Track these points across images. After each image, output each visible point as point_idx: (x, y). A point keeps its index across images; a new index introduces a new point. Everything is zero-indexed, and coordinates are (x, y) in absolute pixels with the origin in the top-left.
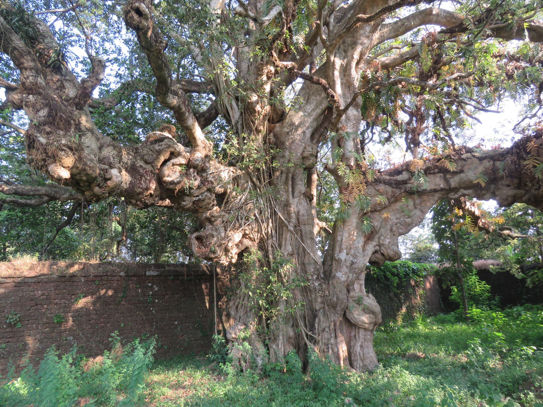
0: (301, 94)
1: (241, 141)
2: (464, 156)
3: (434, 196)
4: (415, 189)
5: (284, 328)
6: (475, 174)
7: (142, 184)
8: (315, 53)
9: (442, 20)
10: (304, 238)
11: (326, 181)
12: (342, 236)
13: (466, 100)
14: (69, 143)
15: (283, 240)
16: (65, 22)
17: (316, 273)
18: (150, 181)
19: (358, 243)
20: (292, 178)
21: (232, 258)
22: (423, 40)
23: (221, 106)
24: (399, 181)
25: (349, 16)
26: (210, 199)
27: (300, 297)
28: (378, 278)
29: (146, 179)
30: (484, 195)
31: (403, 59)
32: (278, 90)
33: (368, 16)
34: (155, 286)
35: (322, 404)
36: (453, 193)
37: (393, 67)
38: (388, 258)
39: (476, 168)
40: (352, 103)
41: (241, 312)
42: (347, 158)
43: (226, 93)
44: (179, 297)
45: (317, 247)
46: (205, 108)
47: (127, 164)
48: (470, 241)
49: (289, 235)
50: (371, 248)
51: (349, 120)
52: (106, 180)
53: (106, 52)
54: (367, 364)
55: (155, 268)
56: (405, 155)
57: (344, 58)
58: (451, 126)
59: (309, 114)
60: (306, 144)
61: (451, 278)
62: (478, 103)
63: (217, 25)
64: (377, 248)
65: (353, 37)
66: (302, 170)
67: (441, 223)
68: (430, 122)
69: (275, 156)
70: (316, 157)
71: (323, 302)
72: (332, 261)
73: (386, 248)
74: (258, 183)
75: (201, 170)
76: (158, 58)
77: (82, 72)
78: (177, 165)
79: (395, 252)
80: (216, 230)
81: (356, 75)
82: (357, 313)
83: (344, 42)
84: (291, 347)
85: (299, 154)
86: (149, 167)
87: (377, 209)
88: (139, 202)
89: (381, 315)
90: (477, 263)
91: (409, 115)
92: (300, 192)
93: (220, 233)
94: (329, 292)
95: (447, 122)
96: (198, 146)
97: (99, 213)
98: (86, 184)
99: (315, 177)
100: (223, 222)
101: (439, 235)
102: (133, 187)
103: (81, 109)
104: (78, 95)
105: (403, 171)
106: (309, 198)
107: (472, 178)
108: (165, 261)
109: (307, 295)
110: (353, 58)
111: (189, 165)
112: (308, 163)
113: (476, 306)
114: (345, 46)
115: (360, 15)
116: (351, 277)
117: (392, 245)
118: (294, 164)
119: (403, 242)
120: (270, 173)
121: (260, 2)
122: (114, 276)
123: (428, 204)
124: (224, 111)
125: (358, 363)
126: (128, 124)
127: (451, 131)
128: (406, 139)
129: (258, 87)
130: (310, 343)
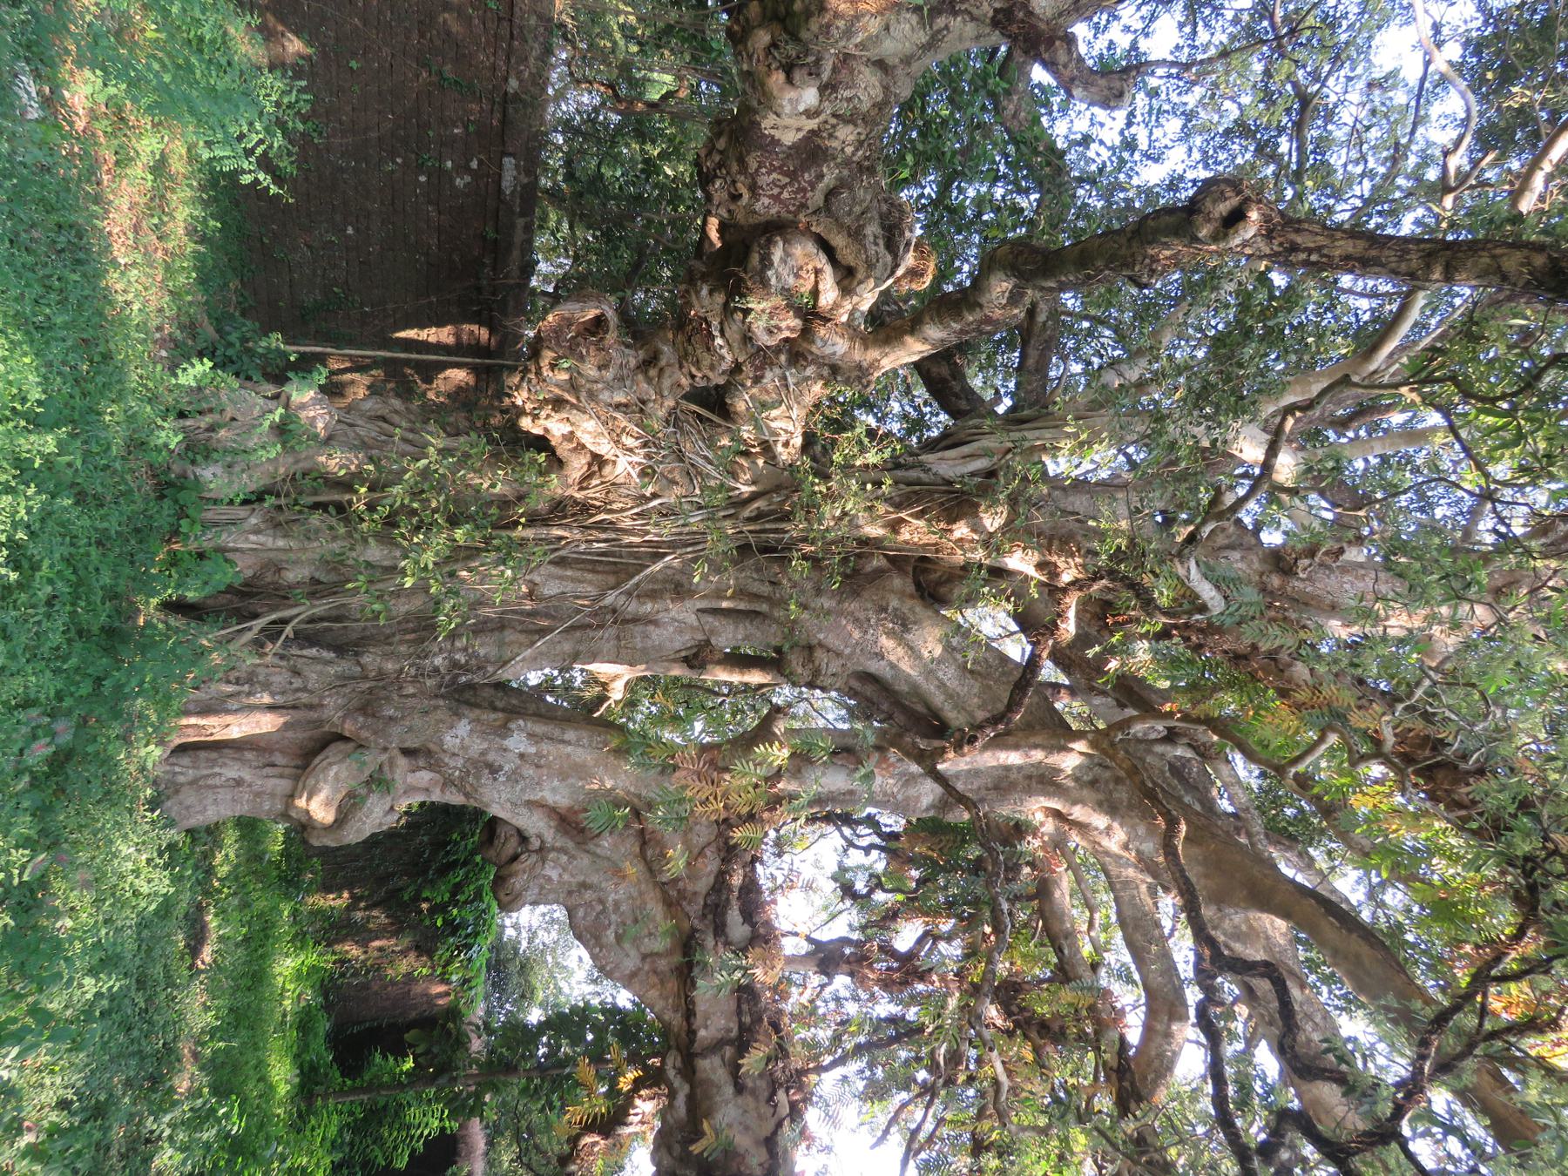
2: (781, 1096)
3: (676, 1011)
4: (698, 957)
5: (309, 555)
6: (730, 1126)
7: (769, 173)
8: (1098, 701)
9: (1153, 1045)
10: (578, 634)
11: (743, 712)
12: (578, 744)
13: (938, 1105)
15: (578, 574)
16: (1246, 17)
17: (473, 662)
18: (776, 198)
19: (554, 790)
20: (757, 613)
21: (535, 417)
22: (1106, 993)
23: (976, 427)
24: (724, 914)
25: (1187, 799)
26: (712, 367)
27: (403, 609)
29: (783, 187)
30: (670, 1150)
31: (1056, 937)
32: (1005, 590)
34: (468, 179)
35: (58, 648)
36: (679, 1064)
37: (1041, 913)
38: (504, 872)
39: (747, 1128)
40: (952, 794)
41: (367, 431)
42: (799, 771)
43: (1010, 445)
44: (429, 247)
46: (977, 382)
47: (831, 136)
48: (542, 1110)
49: (591, 590)
50: (536, 824)
51: (906, 784)
52: (788, 69)
54: (181, 797)
55: (524, 187)
56: (796, 934)
57: (1077, 779)
58: (871, 1065)
59: (931, 672)
60: (850, 657)
61: (436, 1056)
62: (930, 1139)
63: (1194, 437)
64: (536, 844)
65: (1130, 807)
66: (774, 642)
67: (599, 1030)
68: (885, 1008)
69: (821, 569)
70: (811, 685)
71: (381, 675)
72: (503, 710)
74: (746, 513)
75: (796, 352)
76: (1112, 259)
77: (1106, 44)
78: (817, 283)
79: (519, 895)
80: (620, 379)
81: (1036, 809)
82: (344, 774)
83: (1118, 780)
84: (249, 573)
85: (821, 636)
86: (816, 198)
87: (648, 846)
88: (717, 158)
89: (333, 844)
90: (477, 1134)
92: (712, 632)
93: (609, 387)
94: (413, 695)
96: (866, 348)
97: (704, 39)
99: (756, 677)
100: (644, 402)
101: (567, 1023)
102: (762, 148)
103: (995, 23)
104: (1033, 21)
105: (753, 925)
106: (696, 655)
107: (719, 1116)
108: (544, 218)
109: (406, 632)
110: (1075, 803)
111: (811, 315)
112: (795, 662)
113: (348, 1125)
114: (1107, 782)
115: (1183, 827)
116: (452, 763)
117: (542, 888)
118: (795, 622)
120: (774, 550)
121: (1243, 558)
122: (508, 58)
123: (653, 994)
124: (962, 436)
125: (186, 770)
127: (853, 1067)
128: (845, 941)
130: (256, 630)
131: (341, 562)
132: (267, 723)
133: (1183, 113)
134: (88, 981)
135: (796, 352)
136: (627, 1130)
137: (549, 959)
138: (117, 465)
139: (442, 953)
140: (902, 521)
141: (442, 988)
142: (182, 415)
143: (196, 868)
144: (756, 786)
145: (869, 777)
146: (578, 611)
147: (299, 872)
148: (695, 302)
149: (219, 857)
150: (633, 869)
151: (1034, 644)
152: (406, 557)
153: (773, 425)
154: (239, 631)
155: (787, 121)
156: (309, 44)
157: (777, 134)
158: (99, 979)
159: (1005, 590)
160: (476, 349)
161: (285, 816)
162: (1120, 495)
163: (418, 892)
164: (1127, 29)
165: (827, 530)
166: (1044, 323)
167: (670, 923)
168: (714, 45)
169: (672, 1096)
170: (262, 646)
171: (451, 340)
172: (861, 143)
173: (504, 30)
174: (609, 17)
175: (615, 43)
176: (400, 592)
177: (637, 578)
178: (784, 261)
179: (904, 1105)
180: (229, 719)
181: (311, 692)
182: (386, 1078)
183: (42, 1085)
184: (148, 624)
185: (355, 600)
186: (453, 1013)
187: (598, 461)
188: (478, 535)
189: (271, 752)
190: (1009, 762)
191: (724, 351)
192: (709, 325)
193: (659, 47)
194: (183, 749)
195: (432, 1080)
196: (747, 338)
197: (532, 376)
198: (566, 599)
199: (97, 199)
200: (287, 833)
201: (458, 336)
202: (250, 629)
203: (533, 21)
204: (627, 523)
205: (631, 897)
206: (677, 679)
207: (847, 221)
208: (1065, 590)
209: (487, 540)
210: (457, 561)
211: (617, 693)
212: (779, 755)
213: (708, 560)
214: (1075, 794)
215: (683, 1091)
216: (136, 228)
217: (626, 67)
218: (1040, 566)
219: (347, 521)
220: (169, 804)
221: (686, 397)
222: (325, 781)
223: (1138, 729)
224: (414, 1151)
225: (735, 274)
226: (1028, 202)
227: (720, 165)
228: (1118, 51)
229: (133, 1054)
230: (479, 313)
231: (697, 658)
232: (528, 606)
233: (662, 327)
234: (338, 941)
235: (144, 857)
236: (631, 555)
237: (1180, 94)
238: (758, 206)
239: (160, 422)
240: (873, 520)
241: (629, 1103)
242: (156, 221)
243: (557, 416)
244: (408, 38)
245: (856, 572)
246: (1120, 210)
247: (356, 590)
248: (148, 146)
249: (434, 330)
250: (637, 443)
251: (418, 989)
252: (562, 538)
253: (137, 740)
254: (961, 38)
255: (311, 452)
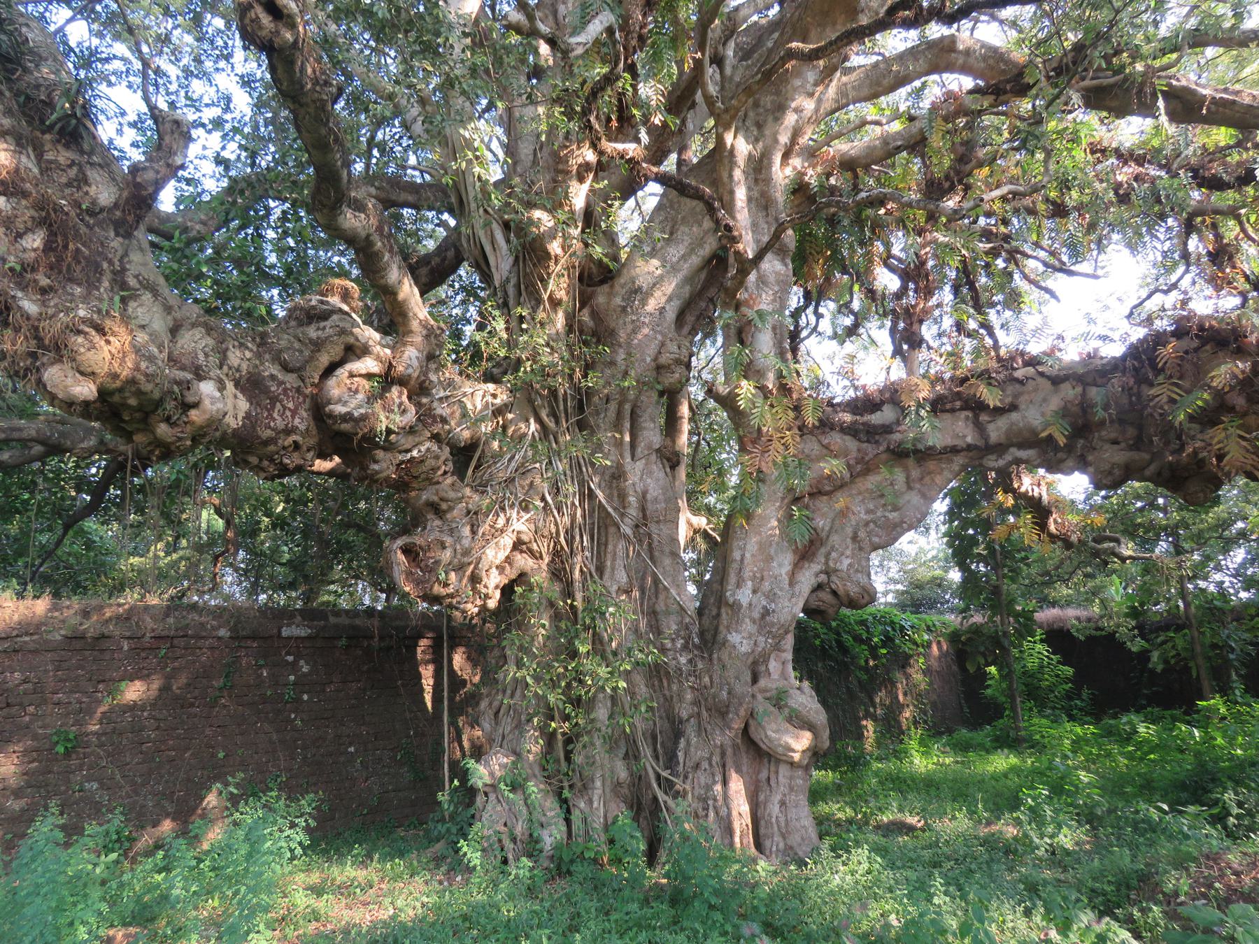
0: (657, 221)
1: (514, 324)
2: (1019, 374)
3: (952, 461)
4: (909, 446)
5: (606, 762)
6: (1043, 415)
7: (274, 420)
8: (690, 126)
9: (976, 65)
10: (656, 554)
11: (711, 424)
12: (743, 549)
14: (95, 316)
15: (609, 556)
16: (95, 26)
17: (682, 633)
18: (294, 413)
19: (780, 565)
20: (633, 412)
21: (487, 596)
22: (934, 108)
24: (874, 426)
25: (770, 44)
26: (437, 457)
28: (823, 647)
29: (285, 408)
31: (888, 151)
32: (603, 208)
33: (811, 46)
34: (302, 662)
35: (688, 938)
36: (993, 457)
38: (845, 600)
39: (1045, 400)
41: (507, 725)
43: (481, 210)
45: (687, 574)
46: (431, 245)
47: (238, 370)
48: (1028, 565)
50: (808, 578)
52: (187, 407)
53: (193, 103)
54: (795, 844)
55: (304, 619)
57: (757, 140)
60: (664, 335)
62: (1052, 253)
64: (823, 577)
65: (778, 93)
66: (655, 396)
67: (966, 524)
68: (946, 295)
70: (688, 366)
71: (696, 703)
72: (719, 608)
73: (842, 579)
74: (551, 424)
75: (418, 390)
77: (134, 149)
78: (360, 375)
80: (451, 532)
82: (774, 726)
83: (756, 105)
85: (648, 359)
86: (291, 380)
88: (266, 463)
90: (1045, 615)
91: (901, 277)
92: (649, 447)
93: (459, 539)
95: (984, 296)
96: (411, 332)
97: (170, 487)
98: (137, 415)
99: (684, 410)
100: (469, 512)
101: (961, 550)
102: (253, 427)
103: (128, 235)
104: (122, 202)
105: (882, 403)
106: (669, 460)
109: (661, 686)
110: (776, 141)
111: (388, 379)
112: (670, 379)
115: (794, 45)
117: (857, 571)
118: (638, 381)
119: (881, 565)
120: (581, 401)
122: (203, 638)
124: (477, 252)
125: (775, 842)
126: (244, 278)
127: (992, 315)
128: (893, 331)
129: (556, 201)
130: (666, 798)
131: (610, 738)
132: (737, 785)
133: (186, 79)
134: (936, 900)
135: (418, 390)
136: (1045, 497)
137: (910, 567)
138: (547, 905)
139: (907, 648)
140: (550, 297)
141: (935, 648)
142: (505, 862)
143: (848, 831)
144: (772, 406)
145: (761, 314)
146: (639, 554)
147: (847, 758)
148: (384, 474)
149: (840, 815)
150: (841, 501)
151: (647, 180)
152: (603, 688)
153: (479, 407)
154: (667, 810)
155: (230, 407)
156: (209, 789)
157: (241, 415)
158: (935, 894)
159: (603, 208)
160: (436, 648)
161: (807, 768)
162: (517, 114)
163: (861, 668)
164: (120, 132)
165: (562, 359)
166: (377, 188)
167: (883, 469)
168: (173, 477)
169: (1018, 462)
170: (678, 792)
171: (431, 668)
172: (242, 345)
173: (181, 642)
174: (161, 564)
175: (181, 558)
176: (630, 691)
177: (610, 510)
178: (345, 404)
179: (1026, 277)
180: (735, 813)
181: (712, 754)
182: (1004, 685)
183: (1013, 928)
184: (667, 876)
185: (638, 725)
186: (954, 637)
187: (518, 545)
188: (583, 635)
189: (758, 781)
190: (744, 198)
191: (423, 449)
192: (403, 462)
193: (180, 522)
194: (759, 846)
195: (1005, 651)
196: (411, 430)
197: (454, 601)
198: (629, 565)
199: (346, 932)
200: (820, 769)
201: (427, 663)
202: (665, 802)
203: (171, 620)
204: (567, 520)
205: (863, 501)
206: (688, 475)
207: (307, 353)
208: (601, 153)
209: (586, 628)
210: (604, 650)
211: (701, 522)
212: (746, 389)
213: (592, 454)
214: (769, 141)
215: (1015, 452)
216: (365, 904)
217: (199, 548)
218: (581, 179)
219: (578, 735)
220: (801, 854)
221: (462, 477)
222: (779, 739)
223: (713, 89)
224: (1059, 662)
225: (360, 442)
226: (277, 208)
227: (272, 460)
228: (139, 138)
229: (989, 867)
230: (407, 647)
231: (671, 460)
232: (636, 594)
233: (407, 501)
234: (900, 727)
235: (842, 868)
236: (591, 516)
237: (170, 83)
238: (302, 427)
239: (512, 877)
240: (552, 322)
241: (1025, 496)
242: (358, 891)
243: (485, 580)
244: (196, 716)
245: (594, 334)
246: (276, 130)
247: (632, 725)
248: (302, 900)
249: (423, 681)
250: (502, 515)
251: (935, 664)
252: (581, 570)
253: (753, 877)
254: (145, 264)
255: (526, 766)
